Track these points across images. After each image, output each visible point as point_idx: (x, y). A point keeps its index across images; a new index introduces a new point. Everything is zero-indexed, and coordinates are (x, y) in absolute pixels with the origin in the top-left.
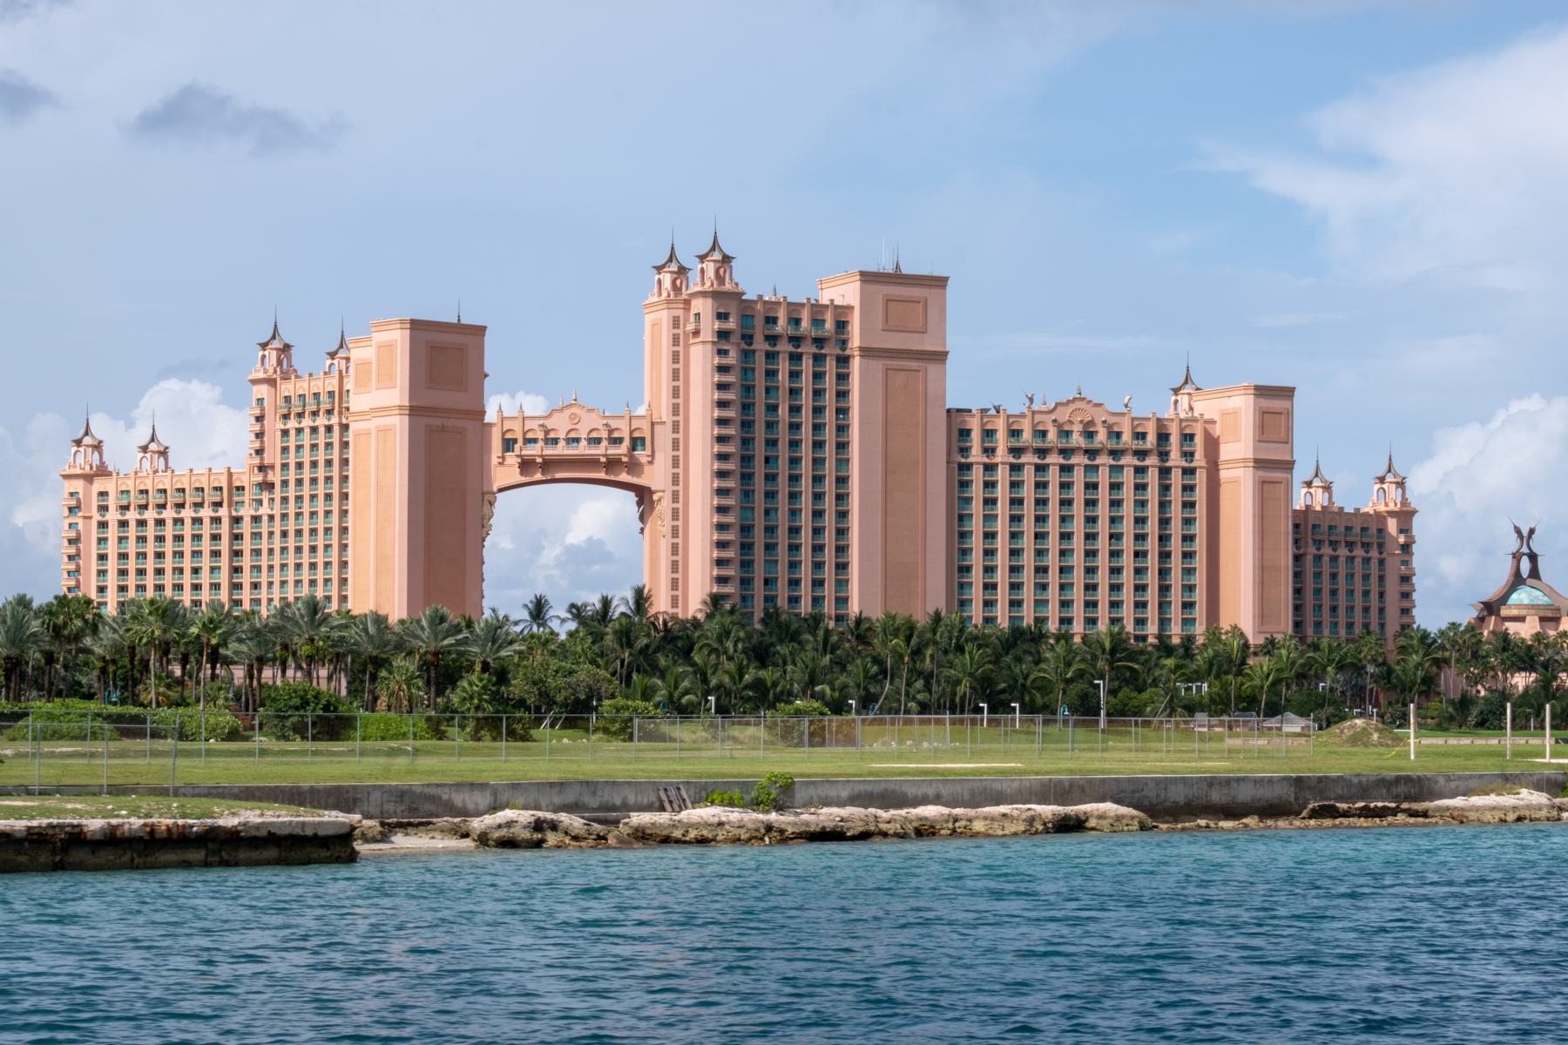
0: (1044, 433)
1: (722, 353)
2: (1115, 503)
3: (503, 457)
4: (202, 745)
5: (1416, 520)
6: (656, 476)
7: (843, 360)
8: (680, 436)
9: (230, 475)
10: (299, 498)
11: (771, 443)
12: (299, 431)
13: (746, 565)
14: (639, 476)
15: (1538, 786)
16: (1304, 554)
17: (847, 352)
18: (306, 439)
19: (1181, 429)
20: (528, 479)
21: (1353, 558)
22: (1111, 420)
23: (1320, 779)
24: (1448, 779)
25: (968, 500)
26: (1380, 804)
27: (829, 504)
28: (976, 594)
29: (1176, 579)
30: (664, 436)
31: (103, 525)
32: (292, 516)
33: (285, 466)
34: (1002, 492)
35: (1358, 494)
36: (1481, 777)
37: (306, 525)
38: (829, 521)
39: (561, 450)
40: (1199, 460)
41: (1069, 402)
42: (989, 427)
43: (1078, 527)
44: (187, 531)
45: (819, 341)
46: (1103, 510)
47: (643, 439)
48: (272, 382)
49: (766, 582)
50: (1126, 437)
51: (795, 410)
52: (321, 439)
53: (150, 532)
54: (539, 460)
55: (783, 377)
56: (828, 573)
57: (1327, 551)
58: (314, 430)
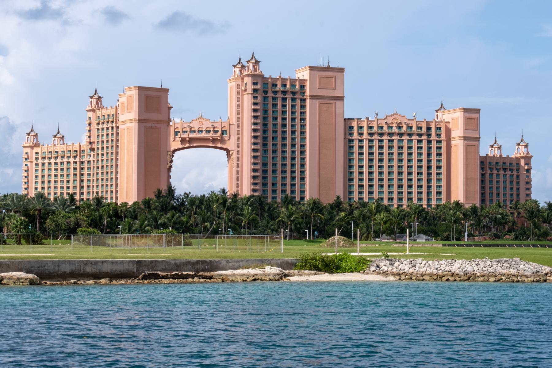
0: (382, 127)
1: (255, 98)
2: (410, 154)
3: (175, 138)
4: (51, 246)
5: (532, 160)
6: (231, 145)
7: (303, 100)
8: (240, 129)
9: (80, 146)
10: (103, 154)
11: (275, 132)
12: (103, 129)
13: (265, 178)
14: (225, 145)
15: (278, 265)
16: (486, 173)
17: (305, 97)
18: (105, 132)
19: (436, 125)
20: (184, 146)
21: (506, 175)
22: (408, 122)
23: (152, 262)
24: (228, 262)
25: (353, 153)
26: (185, 273)
27: (297, 155)
28: (356, 189)
29: (434, 183)
30: (234, 129)
31: (37, 165)
32: (100, 161)
33: (98, 142)
34: (366, 150)
35: (512, 151)
36: (247, 261)
37: (105, 164)
38: (298, 161)
39: (195, 135)
40: (443, 137)
41: (391, 115)
42: (361, 125)
43: (395, 163)
44: (65, 166)
45: (294, 93)
46: (405, 157)
47: (226, 131)
48: (93, 111)
49: (273, 184)
50: (414, 129)
51: (284, 119)
52: (110, 132)
53: (53, 167)
54: (187, 139)
55: (279, 107)
56: (297, 181)
57: (495, 172)
58: (108, 128)
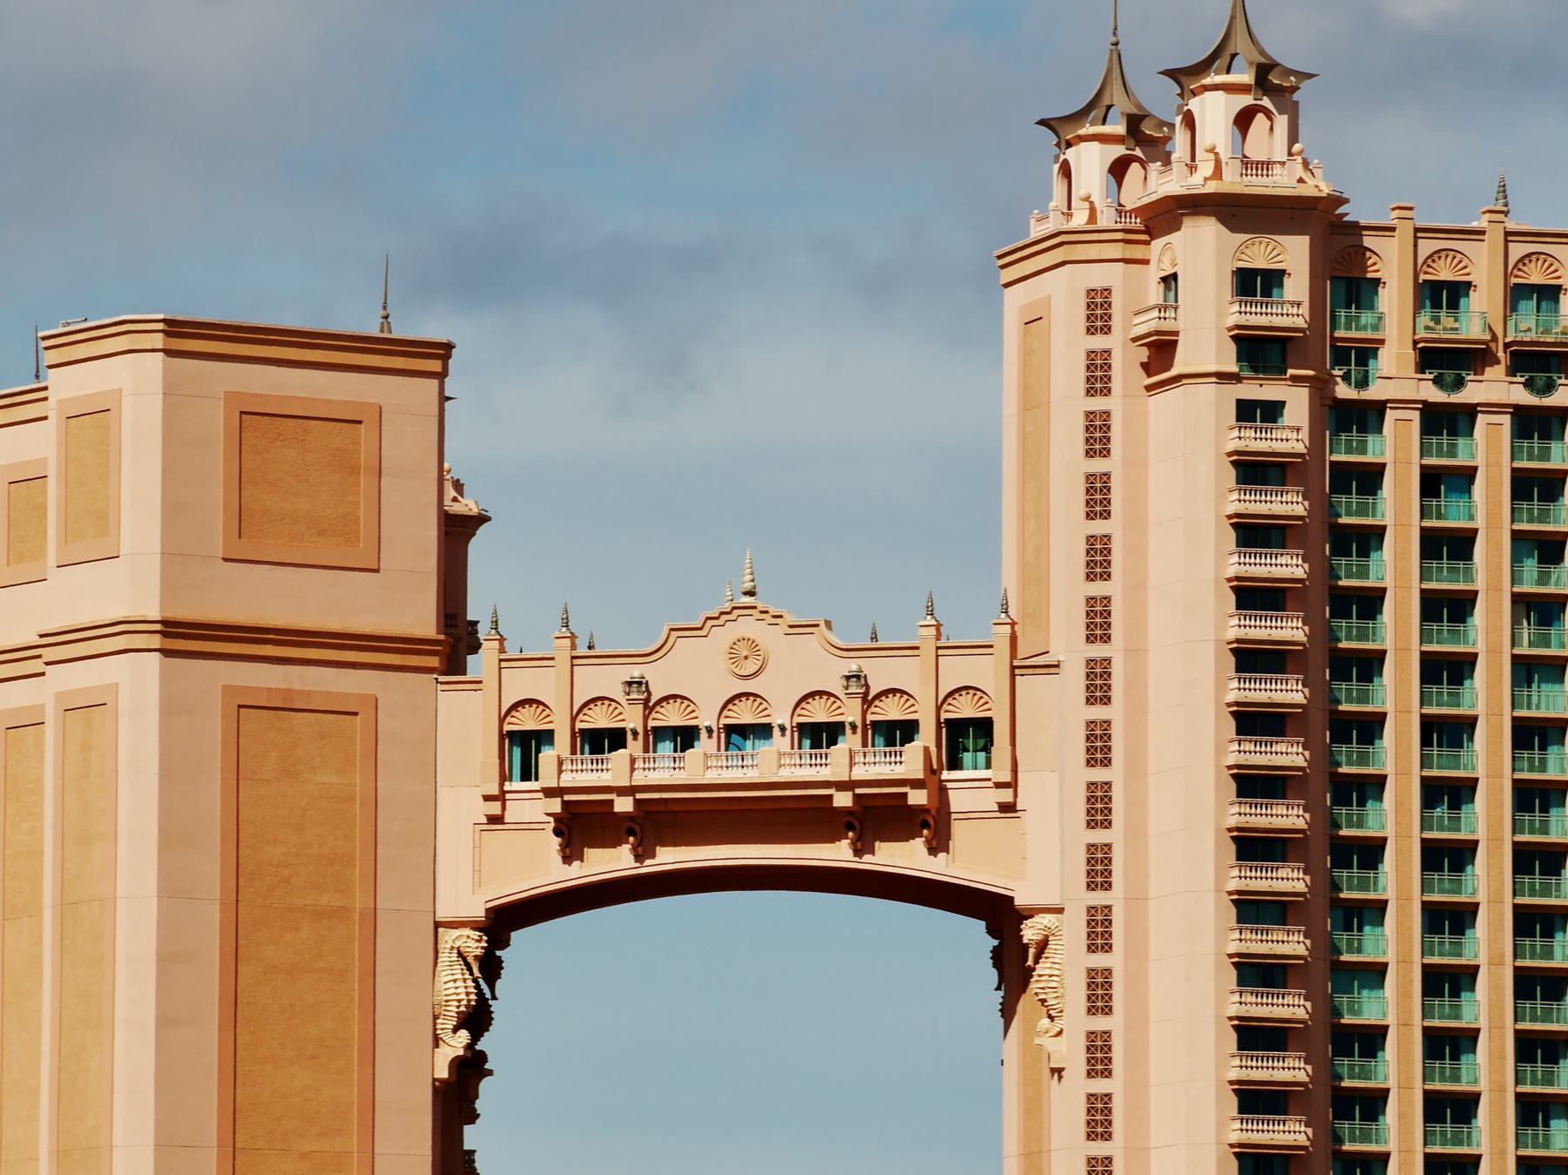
6: (1017, 845)
